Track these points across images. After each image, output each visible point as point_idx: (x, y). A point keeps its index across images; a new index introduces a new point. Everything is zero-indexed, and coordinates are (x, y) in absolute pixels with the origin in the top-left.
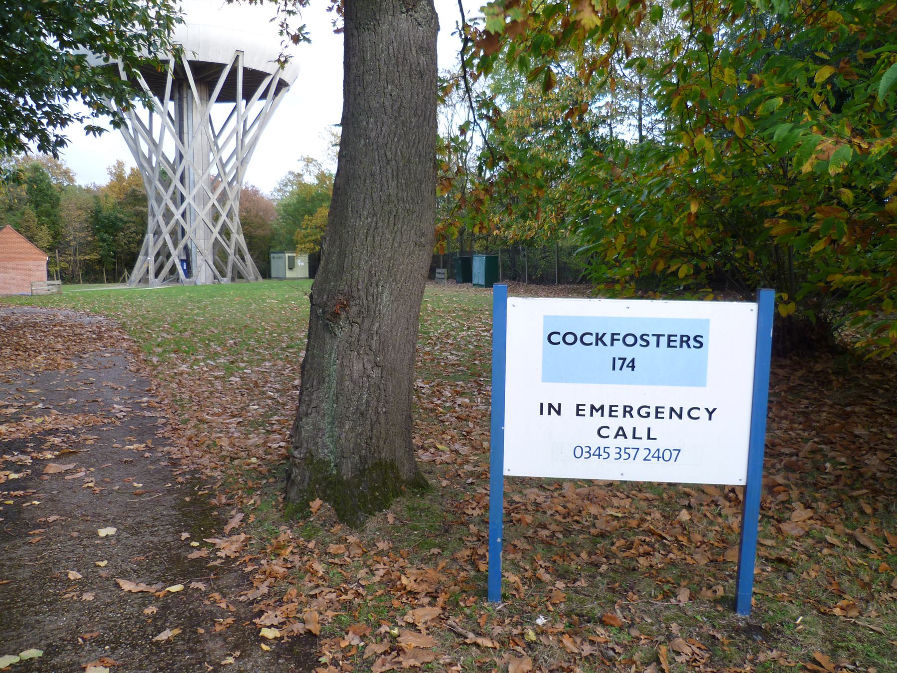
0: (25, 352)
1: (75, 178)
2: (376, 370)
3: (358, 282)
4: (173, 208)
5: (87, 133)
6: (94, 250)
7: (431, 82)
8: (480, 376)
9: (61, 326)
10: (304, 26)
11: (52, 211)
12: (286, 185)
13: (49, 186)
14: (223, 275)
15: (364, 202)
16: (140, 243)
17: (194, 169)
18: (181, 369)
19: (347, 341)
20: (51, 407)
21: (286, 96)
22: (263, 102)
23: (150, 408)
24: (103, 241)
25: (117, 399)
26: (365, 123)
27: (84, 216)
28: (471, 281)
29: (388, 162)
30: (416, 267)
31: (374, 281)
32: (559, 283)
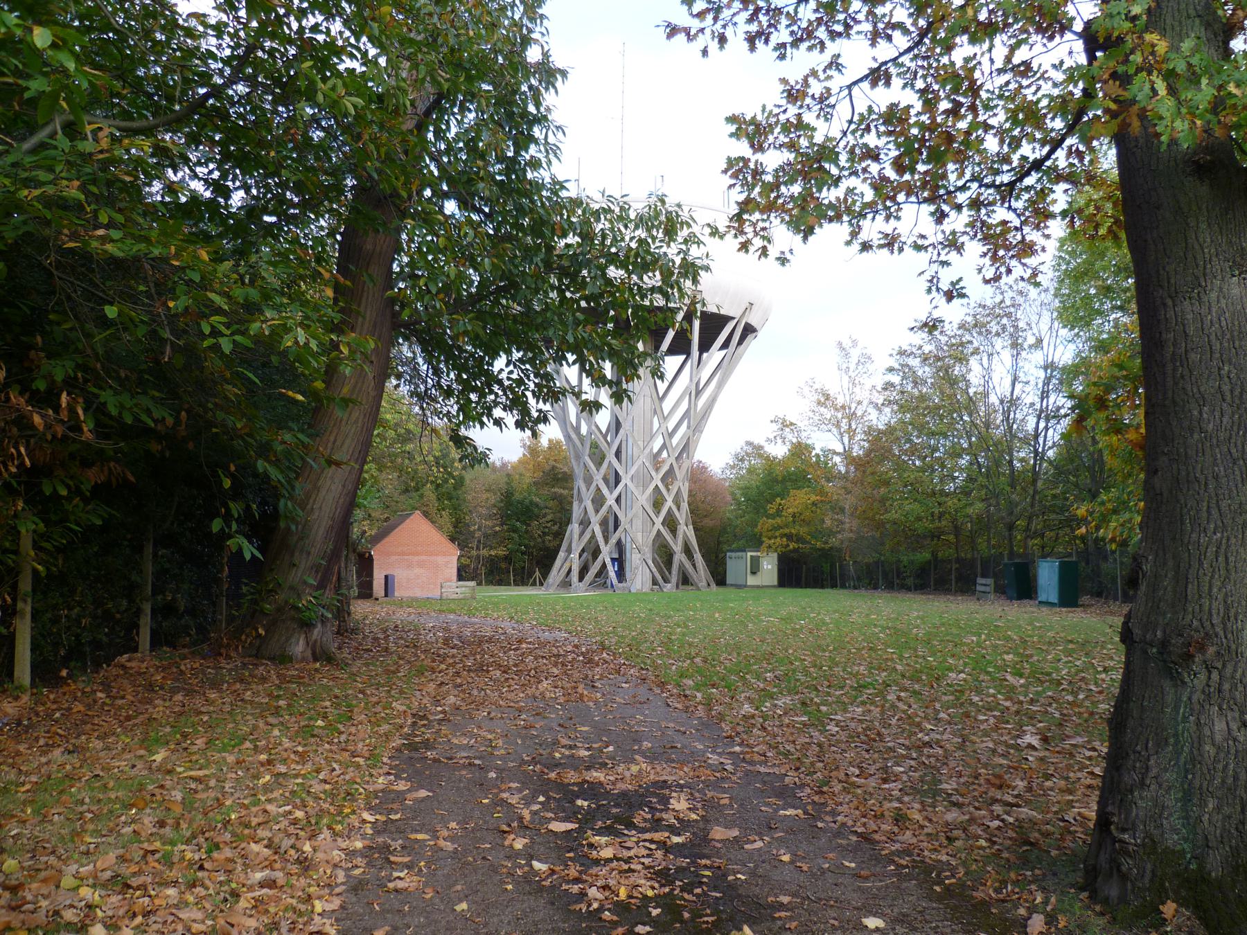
3: (1210, 614)
4: (605, 491)
10: (961, 279)
11: (454, 493)
12: (742, 460)
14: (666, 581)
16: (560, 535)
21: (754, 345)
22: (724, 352)
24: (515, 530)
26: (1195, 413)
28: (1036, 598)
31: (1232, 612)
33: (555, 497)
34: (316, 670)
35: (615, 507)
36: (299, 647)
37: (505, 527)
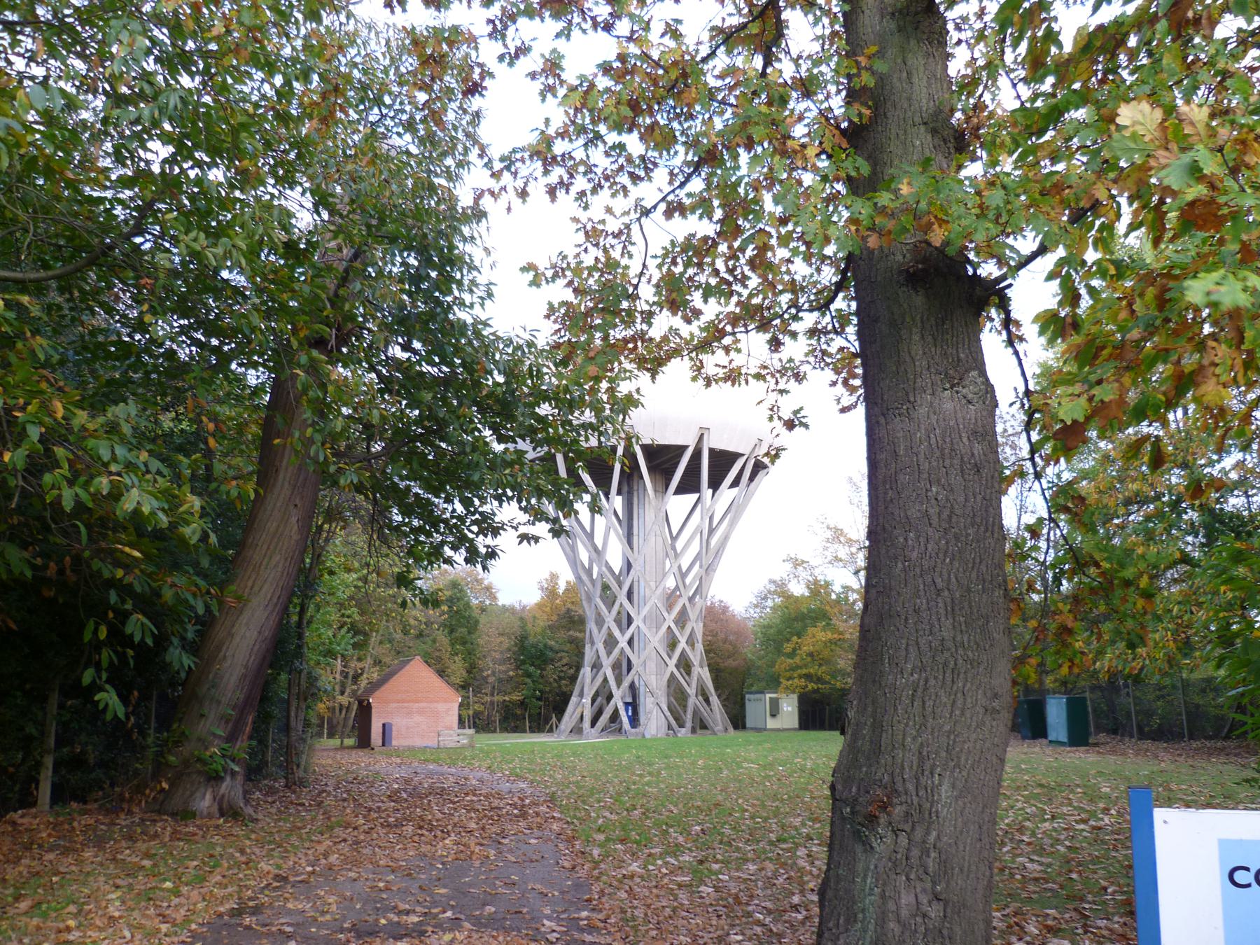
0: (430, 831)
1: (498, 595)
2: (935, 905)
3: (903, 768)
4: (617, 633)
5: (520, 543)
6: (516, 688)
7: (992, 477)
8: (1082, 899)
9: (474, 795)
10: (801, 409)
12: (765, 598)
13: (468, 605)
14: (681, 725)
15: (907, 650)
16: (574, 679)
17: (645, 581)
18: (631, 868)
19: (890, 859)
20: (462, 917)
22: (736, 490)
23: (591, 928)
24: (529, 675)
25: (547, 911)
27: (507, 643)
28: (1045, 736)
29: (939, 592)
30: (988, 744)
31: (927, 766)
32: (1191, 737)
33: (572, 641)
34: (217, 827)
35: (628, 650)
36: (205, 802)
37: (520, 672)
